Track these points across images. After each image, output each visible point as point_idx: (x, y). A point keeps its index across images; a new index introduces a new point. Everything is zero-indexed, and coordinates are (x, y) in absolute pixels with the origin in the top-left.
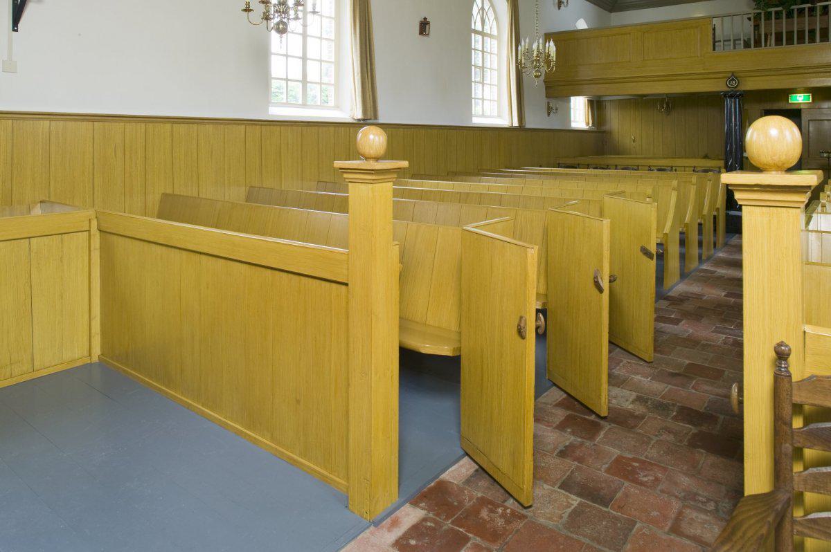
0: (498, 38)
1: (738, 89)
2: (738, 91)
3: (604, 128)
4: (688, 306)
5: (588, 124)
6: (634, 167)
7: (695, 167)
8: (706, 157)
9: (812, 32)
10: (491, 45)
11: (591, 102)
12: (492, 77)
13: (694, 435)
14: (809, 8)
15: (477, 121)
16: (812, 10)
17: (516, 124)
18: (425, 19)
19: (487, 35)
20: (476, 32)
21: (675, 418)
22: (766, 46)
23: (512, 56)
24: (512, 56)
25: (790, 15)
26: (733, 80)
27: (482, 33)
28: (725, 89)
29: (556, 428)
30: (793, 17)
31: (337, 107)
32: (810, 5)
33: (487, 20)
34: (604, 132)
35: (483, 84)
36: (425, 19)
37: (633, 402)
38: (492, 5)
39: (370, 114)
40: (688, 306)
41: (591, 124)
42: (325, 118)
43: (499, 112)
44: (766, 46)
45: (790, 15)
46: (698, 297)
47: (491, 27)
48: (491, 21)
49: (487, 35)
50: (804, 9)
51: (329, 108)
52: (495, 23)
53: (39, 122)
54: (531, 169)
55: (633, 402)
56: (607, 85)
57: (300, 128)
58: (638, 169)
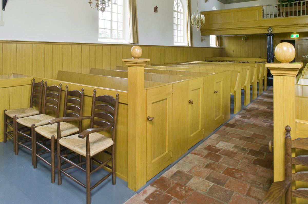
1: (272, 32)
2: (272, 33)
3: (222, 47)
4: (253, 112)
5: (216, 45)
8: (260, 58)
9: (299, 12)
11: (218, 37)
12: (181, 28)
15: (176, 44)
17: (190, 45)
18: (156, 6)
19: (179, 12)
20: (175, 11)
22: (282, 16)
25: (291, 5)
26: (270, 29)
27: (177, 12)
31: (124, 39)
32: (298, 2)
33: (179, 7)
34: (223, 48)
36: (156, 6)
37: (233, 148)
39: (136, 41)
40: (253, 112)
44: (282, 16)
45: (291, 5)
48: (181, 7)
49: (179, 12)
50: (296, 3)
54: (194, 62)
55: (233, 148)
56: (223, 31)
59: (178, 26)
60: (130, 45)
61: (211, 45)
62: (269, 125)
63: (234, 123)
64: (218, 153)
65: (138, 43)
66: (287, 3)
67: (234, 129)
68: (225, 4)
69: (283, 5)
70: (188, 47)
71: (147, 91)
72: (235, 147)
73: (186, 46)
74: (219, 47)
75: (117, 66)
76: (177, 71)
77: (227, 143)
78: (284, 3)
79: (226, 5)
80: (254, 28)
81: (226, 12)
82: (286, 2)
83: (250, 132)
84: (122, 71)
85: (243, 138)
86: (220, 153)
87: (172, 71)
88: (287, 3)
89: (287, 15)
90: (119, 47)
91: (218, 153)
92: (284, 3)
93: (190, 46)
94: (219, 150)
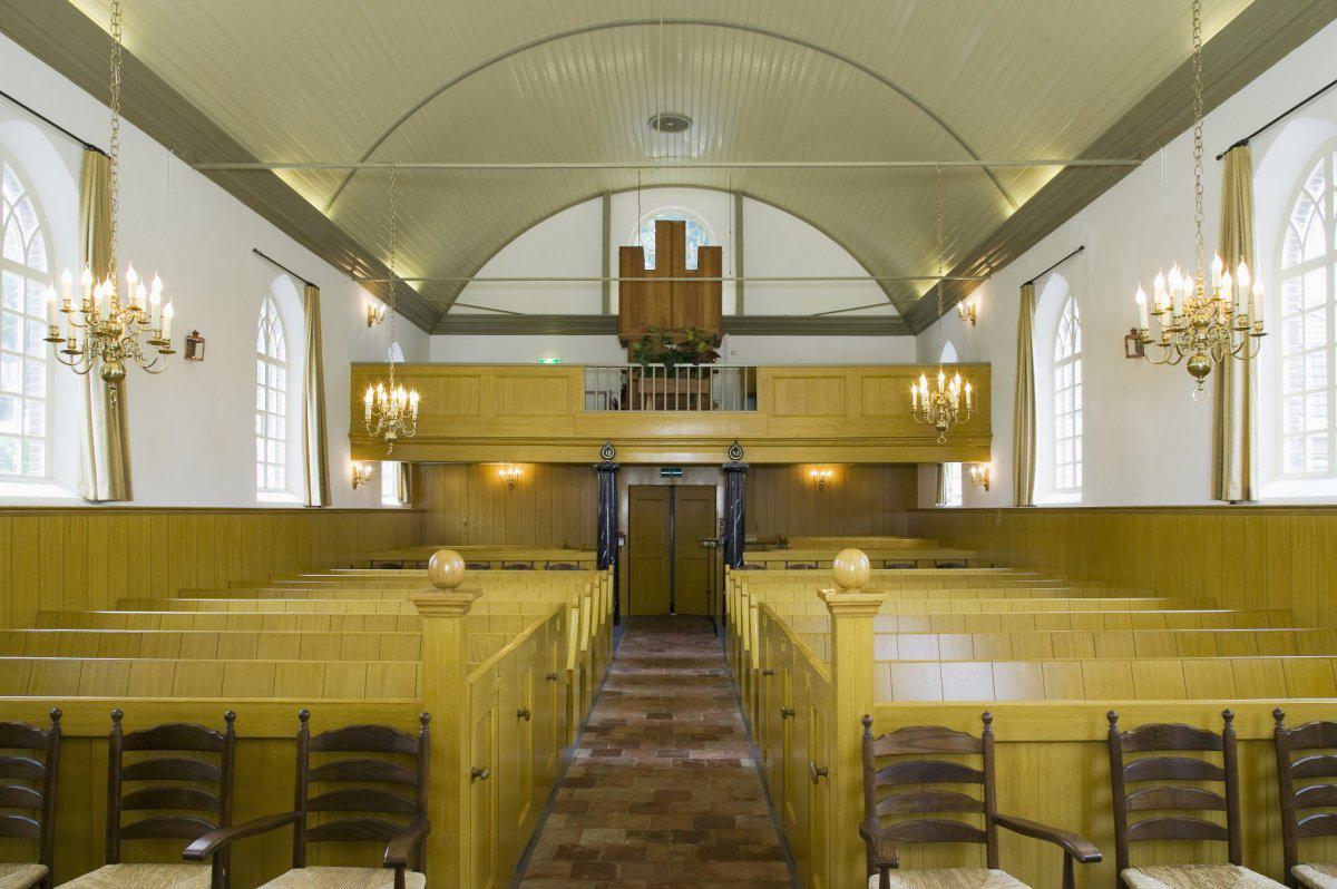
0: (286, 366)
1: (614, 461)
2: (614, 464)
3: (422, 505)
4: (619, 734)
5: (401, 499)
6: (961, 563)
7: (884, 561)
8: (566, 547)
9: (693, 396)
10: (277, 376)
11: (405, 466)
12: (277, 428)
13: (698, 851)
14: (691, 368)
15: (265, 499)
16: (694, 370)
17: (316, 501)
18: (196, 334)
19: (277, 362)
20: (261, 357)
21: (674, 842)
22: (645, 409)
23: (311, 396)
24: (311, 396)
25: (671, 374)
26: (608, 449)
27: (266, 358)
28: (600, 460)
29: (570, 878)
30: (674, 377)
31: (50, 478)
32: (691, 365)
33: (272, 338)
34: (423, 511)
35: (266, 438)
36: (196, 334)
37: (627, 838)
38: (280, 314)
39: (120, 490)
40: (619, 734)
41: (405, 501)
42: (269, 503)
43: (287, 484)
44: (645, 409)
45: (671, 374)
46: (622, 723)
47: (277, 348)
48: (278, 339)
49: (277, 362)
50: (685, 368)
51: (36, 480)
52: (283, 342)
53: (56, 518)
54: (341, 573)
55: (627, 838)
56: (445, 447)
57: (9, 519)
58: (816, 568)
59: (266, 419)
60: (89, 509)
61: (383, 499)
62: (679, 762)
63: (586, 774)
64: (598, 860)
65: (129, 497)
66: (662, 365)
67: (593, 789)
68: (431, 332)
69: (648, 371)
70: (309, 511)
71: (893, 633)
72: (630, 834)
73: (301, 507)
74: (409, 507)
75: (39, 612)
76: (1031, 597)
77: (606, 831)
78: (650, 365)
79: (435, 340)
80: (578, 442)
81: (454, 376)
82: (657, 362)
83: (646, 789)
84: (99, 631)
85: (636, 809)
86: (602, 858)
87: (343, 617)
88: (662, 365)
89: (652, 402)
90: (48, 519)
91: (598, 860)
92: (650, 365)
93: (319, 504)
94: (597, 852)
